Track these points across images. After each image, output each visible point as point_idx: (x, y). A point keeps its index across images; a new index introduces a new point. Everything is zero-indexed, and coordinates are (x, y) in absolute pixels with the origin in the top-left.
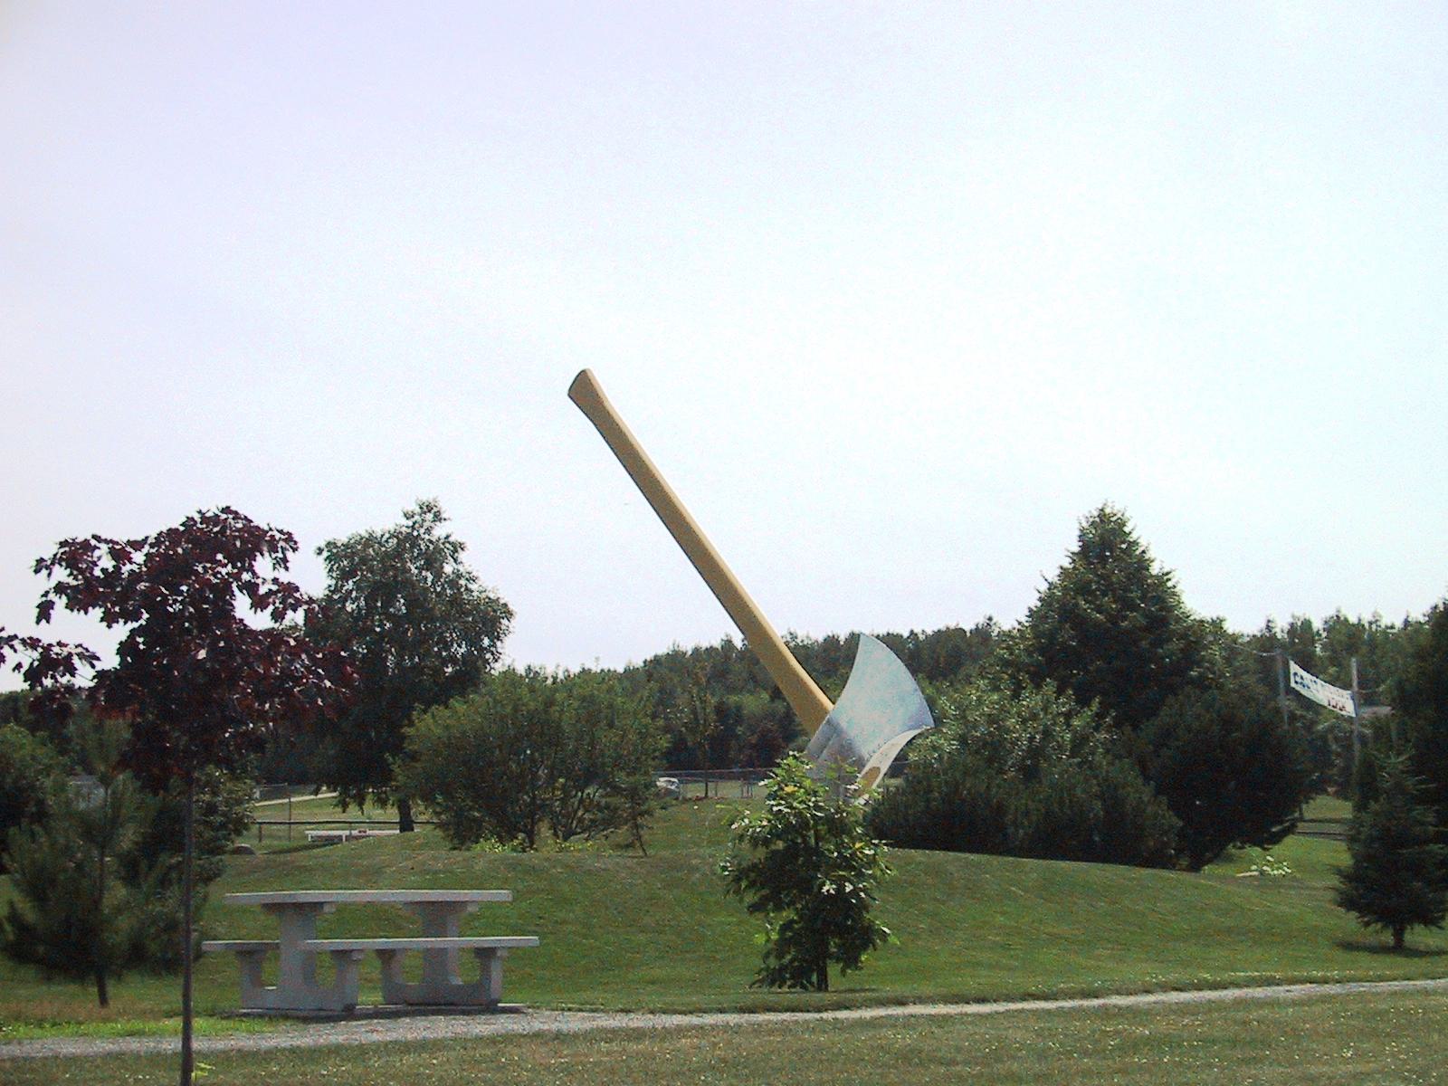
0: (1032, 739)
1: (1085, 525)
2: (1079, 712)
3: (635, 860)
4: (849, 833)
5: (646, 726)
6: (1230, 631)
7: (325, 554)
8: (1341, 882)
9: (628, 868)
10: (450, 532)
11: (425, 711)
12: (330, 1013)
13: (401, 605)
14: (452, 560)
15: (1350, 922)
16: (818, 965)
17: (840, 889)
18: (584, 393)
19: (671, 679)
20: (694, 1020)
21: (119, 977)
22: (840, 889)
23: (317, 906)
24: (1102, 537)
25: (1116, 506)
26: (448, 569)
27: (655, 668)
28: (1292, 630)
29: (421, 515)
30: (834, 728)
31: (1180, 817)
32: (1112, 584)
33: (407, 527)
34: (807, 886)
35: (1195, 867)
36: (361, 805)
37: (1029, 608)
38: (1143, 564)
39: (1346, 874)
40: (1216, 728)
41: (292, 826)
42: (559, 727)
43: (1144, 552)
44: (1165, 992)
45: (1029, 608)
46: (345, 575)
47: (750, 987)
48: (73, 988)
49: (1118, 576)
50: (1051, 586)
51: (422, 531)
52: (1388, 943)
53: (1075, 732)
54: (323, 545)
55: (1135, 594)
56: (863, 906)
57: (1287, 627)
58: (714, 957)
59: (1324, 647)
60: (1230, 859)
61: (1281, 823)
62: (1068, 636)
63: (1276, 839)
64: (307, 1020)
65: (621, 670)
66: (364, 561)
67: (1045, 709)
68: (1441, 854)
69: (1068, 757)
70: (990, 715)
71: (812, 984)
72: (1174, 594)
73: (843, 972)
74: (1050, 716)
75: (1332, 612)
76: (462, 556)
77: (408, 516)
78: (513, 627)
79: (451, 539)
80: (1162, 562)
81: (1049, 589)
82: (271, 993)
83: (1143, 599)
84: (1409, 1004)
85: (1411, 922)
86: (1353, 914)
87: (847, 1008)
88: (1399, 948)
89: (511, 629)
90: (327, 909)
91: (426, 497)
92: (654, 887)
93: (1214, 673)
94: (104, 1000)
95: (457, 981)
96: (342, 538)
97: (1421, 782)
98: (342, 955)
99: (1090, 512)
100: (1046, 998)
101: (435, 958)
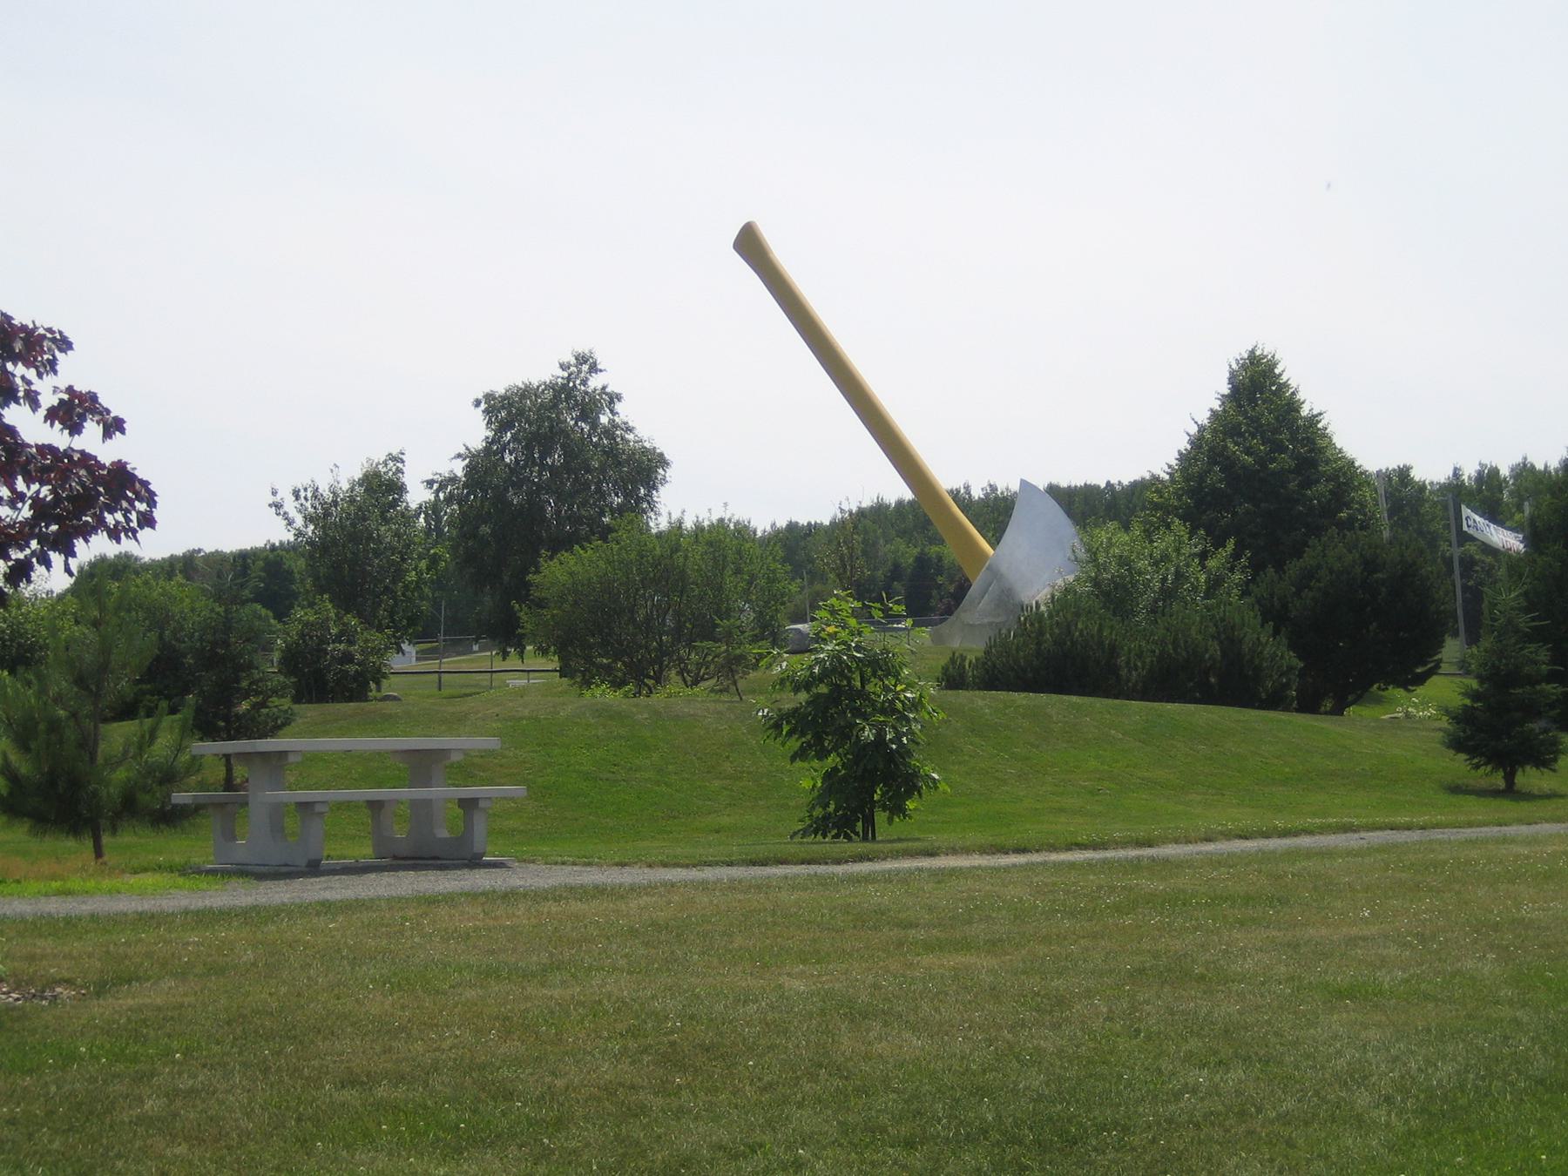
0: (1164, 580)
1: (1235, 366)
2: (1214, 553)
3: (726, 705)
4: (897, 675)
5: (774, 571)
6: (1417, 479)
7: (483, 406)
8: (1450, 723)
9: (692, 715)
10: (606, 383)
11: (551, 558)
12: (292, 868)
13: (556, 458)
14: (608, 411)
15: (1458, 765)
16: (863, 813)
17: (880, 735)
18: (750, 245)
19: (875, 531)
20: (694, 874)
21: (114, 831)
22: (880, 735)
23: (282, 755)
24: (1252, 379)
25: (1268, 346)
26: (604, 419)
27: (859, 520)
28: (1480, 477)
29: (576, 366)
30: (995, 574)
31: (1300, 658)
32: (1262, 425)
33: (562, 378)
34: (846, 733)
35: (1338, 711)
36: (521, 654)
37: (1179, 451)
38: (1293, 406)
39: (1454, 715)
40: (1358, 570)
41: (494, 674)
42: (683, 572)
43: (1293, 393)
44: (1229, 840)
45: (1179, 451)
46: (503, 427)
47: (791, 837)
48: (70, 842)
49: (1268, 418)
50: (1202, 429)
51: (578, 382)
52: (235, 780)
53: (1209, 573)
54: (480, 397)
55: (1284, 436)
56: (905, 752)
57: (1474, 474)
58: (787, 804)
59: (1511, 493)
60: (1379, 701)
61: (1425, 664)
62: (1216, 477)
63: (1421, 680)
64: (261, 877)
65: (827, 523)
66: (521, 412)
67: (1177, 550)
68: (1553, 694)
69: (1203, 598)
70: (1121, 556)
71: (857, 834)
72: (1325, 436)
73: (890, 821)
74: (1182, 558)
75: (1519, 460)
76: (618, 407)
77: (563, 367)
78: (670, 477)
79: (608, 390)
80: (1312, 403)
81: (1199, 431)
82: (242, 849)
83: (1291, 441)
84: (1474, 854)
85: (1522, 764)
86: (1463, 756)
87: (870, 860)
88: (1510, 791)
89: (668, 479)
90: (292, 758)
91: (583, 348)
92: (739, 732)
93: (1365, 515)
94: (99, 853)
95: (443, 833)
96: (500, 390)
97: (1533, 619)
98: (305, 807)
99: (1240, 354)
100: (1095, 847)
101: (422, 809)
